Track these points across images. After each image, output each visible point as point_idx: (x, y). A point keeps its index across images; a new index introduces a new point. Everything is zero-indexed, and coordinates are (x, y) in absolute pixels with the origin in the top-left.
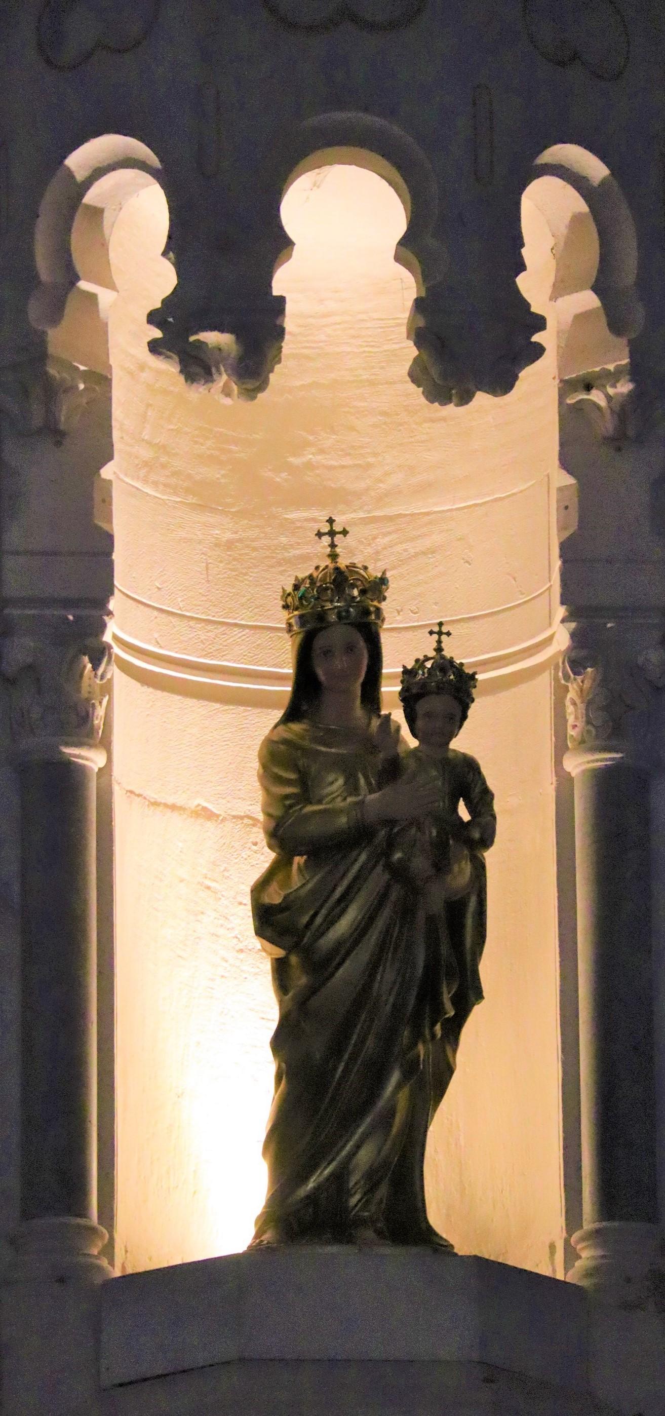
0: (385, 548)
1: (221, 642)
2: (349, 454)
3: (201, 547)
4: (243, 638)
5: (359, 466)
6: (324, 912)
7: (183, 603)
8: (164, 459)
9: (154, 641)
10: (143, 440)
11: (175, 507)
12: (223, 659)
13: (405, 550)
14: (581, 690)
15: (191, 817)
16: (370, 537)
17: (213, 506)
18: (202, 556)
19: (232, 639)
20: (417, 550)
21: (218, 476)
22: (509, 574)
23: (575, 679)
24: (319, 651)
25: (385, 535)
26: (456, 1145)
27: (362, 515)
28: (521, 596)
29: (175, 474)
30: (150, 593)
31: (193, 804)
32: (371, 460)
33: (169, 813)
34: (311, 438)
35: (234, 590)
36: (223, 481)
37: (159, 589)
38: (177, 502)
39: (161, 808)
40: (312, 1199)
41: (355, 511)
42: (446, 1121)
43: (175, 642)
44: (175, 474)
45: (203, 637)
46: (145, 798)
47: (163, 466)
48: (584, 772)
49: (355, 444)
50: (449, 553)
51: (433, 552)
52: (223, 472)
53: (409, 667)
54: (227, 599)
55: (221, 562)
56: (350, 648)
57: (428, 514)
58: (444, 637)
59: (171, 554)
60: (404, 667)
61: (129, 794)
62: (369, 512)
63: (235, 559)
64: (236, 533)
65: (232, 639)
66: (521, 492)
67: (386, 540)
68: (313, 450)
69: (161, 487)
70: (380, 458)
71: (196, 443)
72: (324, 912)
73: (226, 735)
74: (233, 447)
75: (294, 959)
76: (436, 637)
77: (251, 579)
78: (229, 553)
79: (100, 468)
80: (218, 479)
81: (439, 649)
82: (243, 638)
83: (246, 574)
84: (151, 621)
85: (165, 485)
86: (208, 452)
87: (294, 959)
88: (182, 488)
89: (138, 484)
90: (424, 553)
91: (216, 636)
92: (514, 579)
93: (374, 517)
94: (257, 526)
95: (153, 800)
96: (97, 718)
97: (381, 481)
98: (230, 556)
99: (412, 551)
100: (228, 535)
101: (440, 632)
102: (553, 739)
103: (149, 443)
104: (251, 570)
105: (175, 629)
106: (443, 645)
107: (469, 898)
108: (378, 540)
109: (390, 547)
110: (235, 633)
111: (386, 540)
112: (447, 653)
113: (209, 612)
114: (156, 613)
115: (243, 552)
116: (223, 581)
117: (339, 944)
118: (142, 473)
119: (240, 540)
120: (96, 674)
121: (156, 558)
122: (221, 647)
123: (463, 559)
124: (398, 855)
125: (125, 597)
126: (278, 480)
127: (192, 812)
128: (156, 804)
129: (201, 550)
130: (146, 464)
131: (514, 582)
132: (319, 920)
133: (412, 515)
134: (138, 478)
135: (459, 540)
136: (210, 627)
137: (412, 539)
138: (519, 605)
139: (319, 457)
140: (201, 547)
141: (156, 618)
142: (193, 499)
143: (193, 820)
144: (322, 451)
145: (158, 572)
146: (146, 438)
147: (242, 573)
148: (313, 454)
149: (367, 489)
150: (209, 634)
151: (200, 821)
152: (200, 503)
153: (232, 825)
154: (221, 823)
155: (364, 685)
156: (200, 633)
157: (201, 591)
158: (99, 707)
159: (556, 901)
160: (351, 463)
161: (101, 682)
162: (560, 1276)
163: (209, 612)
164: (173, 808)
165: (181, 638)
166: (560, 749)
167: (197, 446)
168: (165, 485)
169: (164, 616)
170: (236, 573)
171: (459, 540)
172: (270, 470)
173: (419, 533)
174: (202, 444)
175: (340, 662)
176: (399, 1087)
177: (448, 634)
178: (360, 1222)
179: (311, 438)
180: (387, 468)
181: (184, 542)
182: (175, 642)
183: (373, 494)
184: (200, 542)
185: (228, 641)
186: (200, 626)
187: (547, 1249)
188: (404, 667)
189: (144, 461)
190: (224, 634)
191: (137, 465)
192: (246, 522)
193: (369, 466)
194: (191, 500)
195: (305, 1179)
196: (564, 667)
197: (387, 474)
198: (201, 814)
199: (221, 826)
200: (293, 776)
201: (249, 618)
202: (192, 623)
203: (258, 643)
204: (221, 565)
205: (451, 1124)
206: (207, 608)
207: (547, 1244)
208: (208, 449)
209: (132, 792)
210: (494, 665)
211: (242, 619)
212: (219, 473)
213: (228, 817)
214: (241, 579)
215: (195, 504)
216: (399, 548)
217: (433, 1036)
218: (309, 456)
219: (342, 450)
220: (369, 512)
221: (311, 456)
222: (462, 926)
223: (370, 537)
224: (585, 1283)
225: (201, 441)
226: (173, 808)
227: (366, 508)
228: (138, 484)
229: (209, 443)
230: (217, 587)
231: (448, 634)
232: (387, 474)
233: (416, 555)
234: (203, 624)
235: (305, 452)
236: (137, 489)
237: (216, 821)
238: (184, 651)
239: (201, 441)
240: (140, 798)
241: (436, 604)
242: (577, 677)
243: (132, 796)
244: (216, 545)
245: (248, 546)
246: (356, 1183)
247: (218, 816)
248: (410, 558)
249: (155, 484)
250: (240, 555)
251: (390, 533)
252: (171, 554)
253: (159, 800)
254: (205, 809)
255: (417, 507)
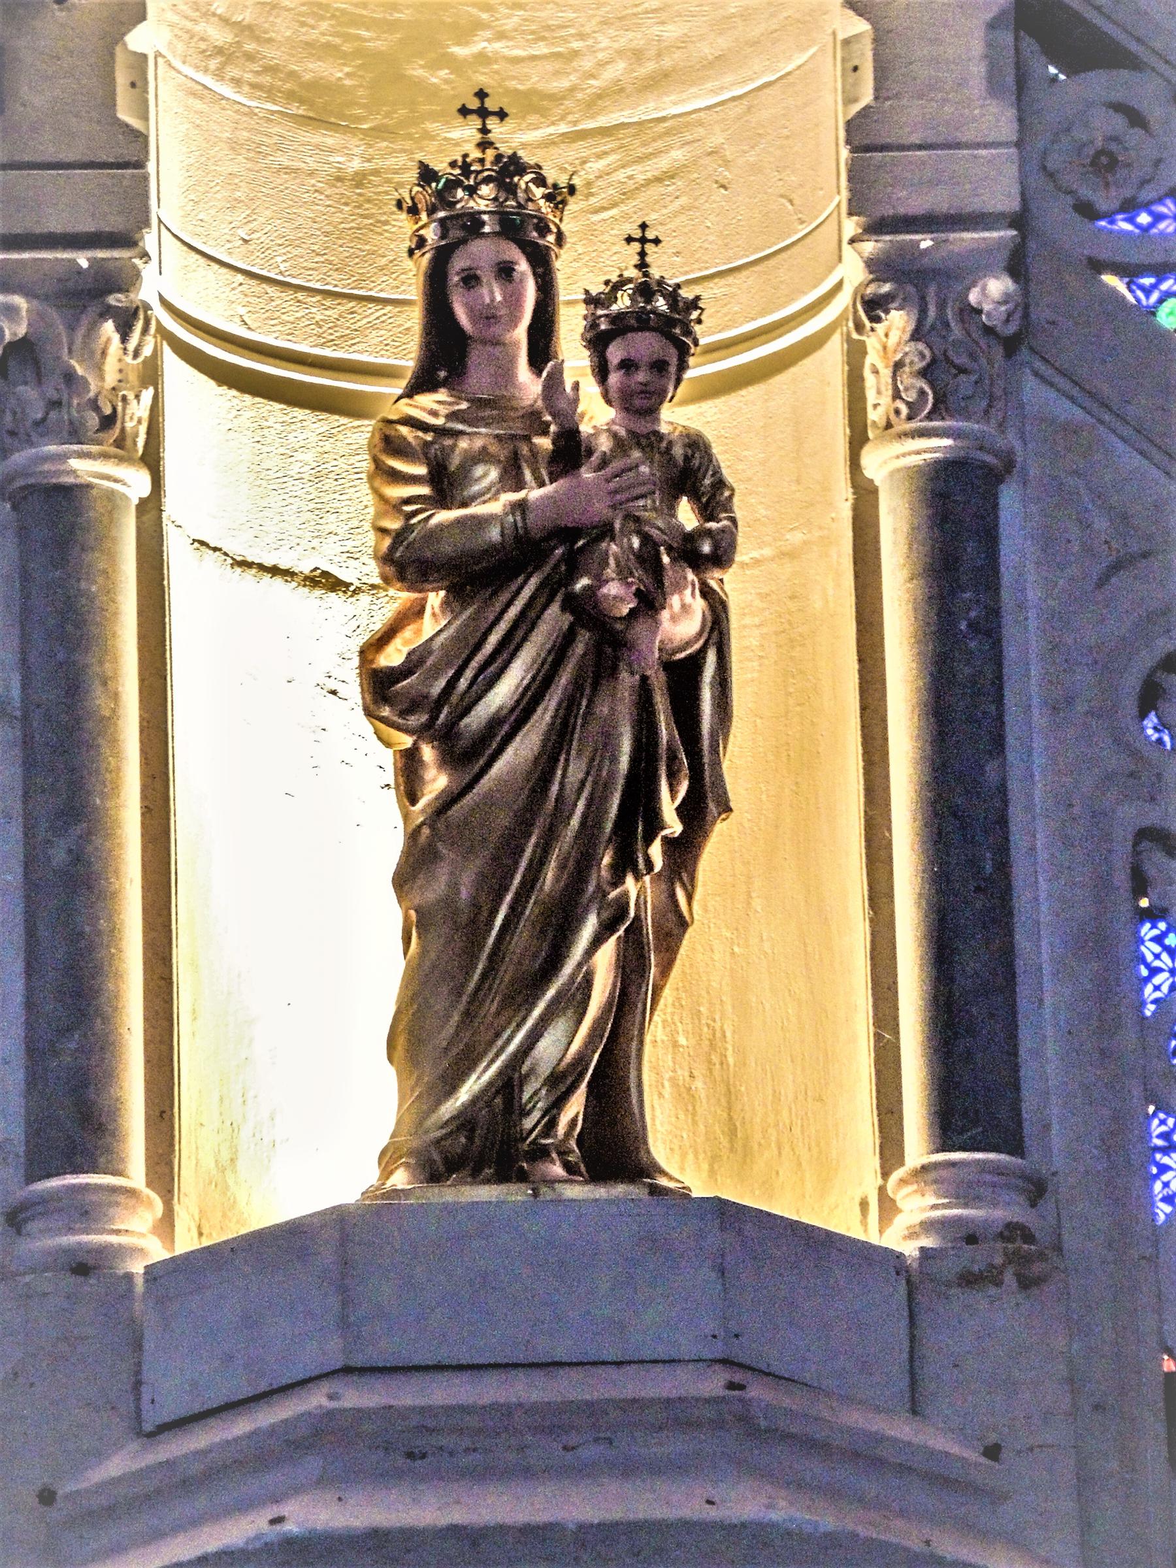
0: (601, 177)
1: (348, 325)
2: (543, 39)
3: (313, 182)
4: (382, 319)
5: (558, 55)
6: (469, 673)
7: (287, 264)
8: (250, 46)
9: (238, 320)
10: (214, 14)
11: (269, 120)
12: (351, 350)
13: (630, 177)
14: (885, 348)
15: (305, 586)
16: (577, 162)
17: (333, 120)
18: (316, 195)
19: (365, 321)
20: (649, 175)
21: (340, 75)
22: (782, 196)
23: (873, 330)
24: (456, 279)
25: (599, 156)
26: (722, 1064)
27: (563, 128)
28: (800, 227)
29: (267, 69)
30: (229, 245)
31: (305, 568)
32: (576, 45)
33: (267, 577)
34: (485, 16)
35: (367, 247)
36: (347, 82)
37: (246, 241)
38: (273, 112)
39: (254, 571)
40: (465, 1121)
41: (553, 124)
42: (705, 1029)
43: (273, 322)
44: (267, 69)
45: (318, 317)
46: (226, 554)
47: (250, 57)
48: (892, 474)
49: (551, 22)
50: (696, 175)
51: (672, 177)
52: (347, 69)
53: (594, 293)
54: (357, 260)
55: (346, 204)
56: (505, 271)
57: (663, 119)
58: (649, 248)
59: (263, 190)
60: (587, 292)
61: (196, 545)
62: (575, 123)
63: (369, 201)
64: (369, 161)
65: (365, 321)
66: (799, 67)
67: (601, 164)
68: (488, 34)
69: (246, 89)
70: (590, 42)
71: (303, 24)
72: (469, 673)
73: (358, 465)
74: (364, 33)
75: (428, 753)
76: (636, 246)
77: (393, 230)
78: (358, 191)
79: (124, 34)
80: (340, 79)
81: (642, 265)
82: (382, 319)
83: (386, 223)
84: (233, 289)
85: (254, 86)
86: (323, 40)
87: (428, 753)
88: (280, 92)
89: (208, 81)
90: (658, 180)
91: (340, 316)
92: (791, 202)
93: (582, 130)
94: (404, 151)
95: (239, 559)
96: (131, 418)
97: (593, 76)
98: (360, 195)
99: (640, 178)
100: (356, 165)
101: (643, 239)
102: (848, 431)
103: (225, 21)
104: (394, 217)
105: (273, 304)
106: (648, 259)
107: (704, 658)
108: (589, 165)
109: (608, 174)
110: (370, 311)
111: (601, 164)
112: (655, 273)
113: (329, 279)
114: (240, 278)
115: (380, 189)
116: (350, 232)
117: (495, 722)
118: (213, 64)
119: (376, 172)
120: (125, 349)
121: (239, 194)
122: (348, 332)
123: (717, 182)
124: (584, 582)
125: (185, 248)
126: (434, 80)
127: (306, 578)
128: (245, 564)
129: (313, 186)
130: (219, 51)
131: (790, 207)
132: (463, 683)
133: (640, 123)
134: (206, 70)
135: (710, 154)
136: (328, 302)
137: (640, 160)
138: (799, 240)
139: (497, 45)
140: (313, 182)
141: (241, 284)
142: (298, 108)
143: (306, 590)
144: (501, 36)
145: (244, 215)
146: (219, 12)
147: (379, 221)
148: (488, 40)
149: (573, 89)
150: (327, 313)
151: (318, 592)
152: (311, 114)
153: (370, 598)
154: (352, 596)
155: (531, 330)
156: (314, 310)
157: (315, 247)
158: (135, 401)
159: (857, 676)
160: (546, 51)
161: (135, 362)
162: (874, 1238)
163: (329, 279)
164: (275, 571)
165: (284, 317)
166: (858, 440)
167: (304, 30)
168: (254, 86)
169: (253, 282)
170: (371, 221)
171: (710, 154)
172: (422, 67)
173: (650, 150)
174: (313, 27)
175: (494, 292)
176: (597, 942)
177: (657, 241)
178: (540, 1153)
179: (485, 16)
180: (600, 55)
181: (286, 173)
182: (273, 322)
183: (580, 96)
184: (312, 174)
185: (359, 324)
186: (314, 299)
187: (857, 1209)
188: (587, 292)
189: (215, 47)
190: (352, 313)
191: (204, 51)
192: (385, 144)
193: (575, 54)
194: (296, 109)
195: (452, 1088)
196: (855, 312)
197: (602, 65)
198: (320, 582)
199: (351, 600)
200: (421, 470)
201: (393, 288)
202: (300, 296)
203: (407, 326)
204: (347, 209)
205: (714, 1035)
206: (325, 274)
207: (857, 1201)
208: (323, 34)
209: (202, 543)
210: (764, 338)
211: (381, 290)
212: (341, 71)
213: (364, 587)
214: (379, 230)
215: (303, 116)
216: (621, 175)
217: (649, 865)
218: (479, 45)
219: (533, 32)
220: (575, 123)
221: (485, 44)
222: (696, 699)
223: (577, 162)
224: (910, 1249)
225: (311, 21)
226: (275, 571)
227: (570, 118)
228: (208, 81)
229: (324, 25)
230: (341, 242)
231: (657, 241)
232: (602, 65)
233: (648, 182)
234: (318, 298)
235: (475, 38)
236: (205, 87)
237: (345, 592)
238: (290, 337)
239: (311, 21)
240: (218, 553)
241: (677, 254)
242: (875, 325)
243: (203, 548)
244: (339, 179)
245: (389, 181)
246: (531, 1097)
247: (348, 585)
248: (637, 189)
249: (237, 82)
250: (379, 193)
251: (606, 153)
252: (263, 190)
253: (250, 559)
254: (325, 574)
255: (647, 109)
